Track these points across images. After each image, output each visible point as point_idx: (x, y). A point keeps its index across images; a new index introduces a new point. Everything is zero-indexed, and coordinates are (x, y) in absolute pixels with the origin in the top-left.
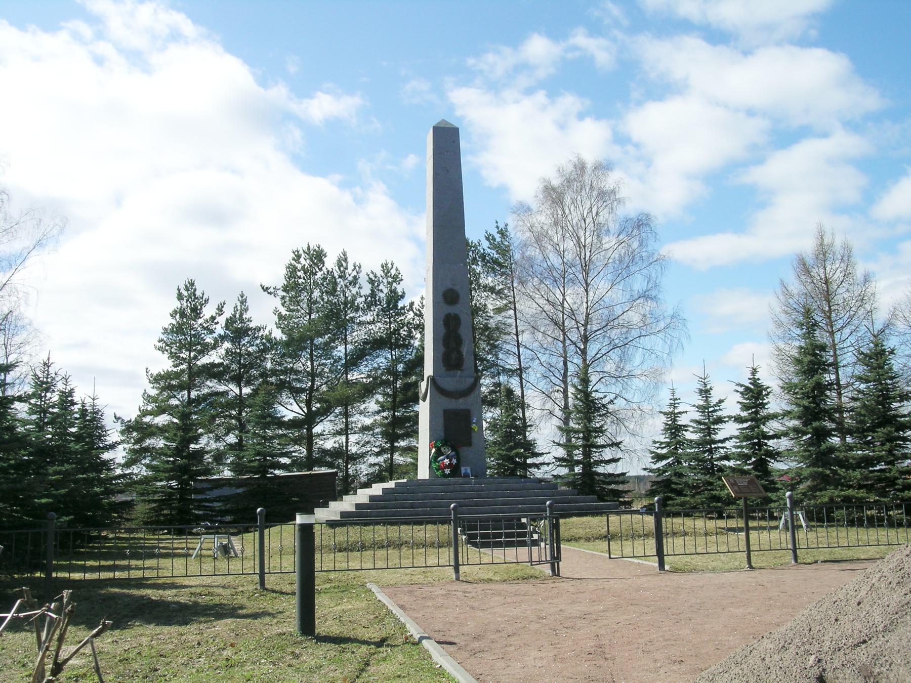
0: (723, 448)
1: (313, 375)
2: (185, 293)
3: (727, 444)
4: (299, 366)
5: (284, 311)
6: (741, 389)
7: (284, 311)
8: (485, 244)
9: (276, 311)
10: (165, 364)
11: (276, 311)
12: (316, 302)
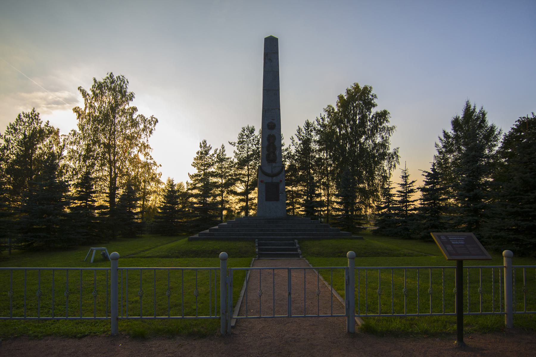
0: (413, 205)
1: (249, 175)
2: (202, 145)
3: (415, 203)
4: (243, 172)
5: (238, 152)
6: (426, 174)
7: (238, 152)
8: (316, 123)
9: (234, 152)
10: (195, 171)
11: (234, 152)
12: (250, 148)
